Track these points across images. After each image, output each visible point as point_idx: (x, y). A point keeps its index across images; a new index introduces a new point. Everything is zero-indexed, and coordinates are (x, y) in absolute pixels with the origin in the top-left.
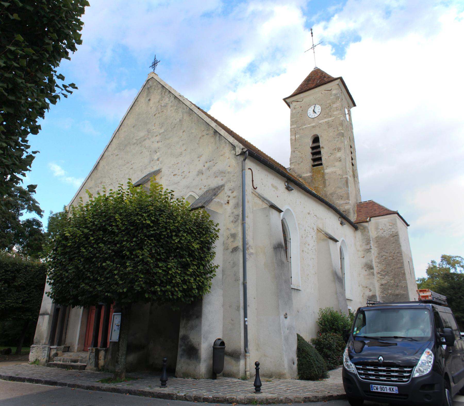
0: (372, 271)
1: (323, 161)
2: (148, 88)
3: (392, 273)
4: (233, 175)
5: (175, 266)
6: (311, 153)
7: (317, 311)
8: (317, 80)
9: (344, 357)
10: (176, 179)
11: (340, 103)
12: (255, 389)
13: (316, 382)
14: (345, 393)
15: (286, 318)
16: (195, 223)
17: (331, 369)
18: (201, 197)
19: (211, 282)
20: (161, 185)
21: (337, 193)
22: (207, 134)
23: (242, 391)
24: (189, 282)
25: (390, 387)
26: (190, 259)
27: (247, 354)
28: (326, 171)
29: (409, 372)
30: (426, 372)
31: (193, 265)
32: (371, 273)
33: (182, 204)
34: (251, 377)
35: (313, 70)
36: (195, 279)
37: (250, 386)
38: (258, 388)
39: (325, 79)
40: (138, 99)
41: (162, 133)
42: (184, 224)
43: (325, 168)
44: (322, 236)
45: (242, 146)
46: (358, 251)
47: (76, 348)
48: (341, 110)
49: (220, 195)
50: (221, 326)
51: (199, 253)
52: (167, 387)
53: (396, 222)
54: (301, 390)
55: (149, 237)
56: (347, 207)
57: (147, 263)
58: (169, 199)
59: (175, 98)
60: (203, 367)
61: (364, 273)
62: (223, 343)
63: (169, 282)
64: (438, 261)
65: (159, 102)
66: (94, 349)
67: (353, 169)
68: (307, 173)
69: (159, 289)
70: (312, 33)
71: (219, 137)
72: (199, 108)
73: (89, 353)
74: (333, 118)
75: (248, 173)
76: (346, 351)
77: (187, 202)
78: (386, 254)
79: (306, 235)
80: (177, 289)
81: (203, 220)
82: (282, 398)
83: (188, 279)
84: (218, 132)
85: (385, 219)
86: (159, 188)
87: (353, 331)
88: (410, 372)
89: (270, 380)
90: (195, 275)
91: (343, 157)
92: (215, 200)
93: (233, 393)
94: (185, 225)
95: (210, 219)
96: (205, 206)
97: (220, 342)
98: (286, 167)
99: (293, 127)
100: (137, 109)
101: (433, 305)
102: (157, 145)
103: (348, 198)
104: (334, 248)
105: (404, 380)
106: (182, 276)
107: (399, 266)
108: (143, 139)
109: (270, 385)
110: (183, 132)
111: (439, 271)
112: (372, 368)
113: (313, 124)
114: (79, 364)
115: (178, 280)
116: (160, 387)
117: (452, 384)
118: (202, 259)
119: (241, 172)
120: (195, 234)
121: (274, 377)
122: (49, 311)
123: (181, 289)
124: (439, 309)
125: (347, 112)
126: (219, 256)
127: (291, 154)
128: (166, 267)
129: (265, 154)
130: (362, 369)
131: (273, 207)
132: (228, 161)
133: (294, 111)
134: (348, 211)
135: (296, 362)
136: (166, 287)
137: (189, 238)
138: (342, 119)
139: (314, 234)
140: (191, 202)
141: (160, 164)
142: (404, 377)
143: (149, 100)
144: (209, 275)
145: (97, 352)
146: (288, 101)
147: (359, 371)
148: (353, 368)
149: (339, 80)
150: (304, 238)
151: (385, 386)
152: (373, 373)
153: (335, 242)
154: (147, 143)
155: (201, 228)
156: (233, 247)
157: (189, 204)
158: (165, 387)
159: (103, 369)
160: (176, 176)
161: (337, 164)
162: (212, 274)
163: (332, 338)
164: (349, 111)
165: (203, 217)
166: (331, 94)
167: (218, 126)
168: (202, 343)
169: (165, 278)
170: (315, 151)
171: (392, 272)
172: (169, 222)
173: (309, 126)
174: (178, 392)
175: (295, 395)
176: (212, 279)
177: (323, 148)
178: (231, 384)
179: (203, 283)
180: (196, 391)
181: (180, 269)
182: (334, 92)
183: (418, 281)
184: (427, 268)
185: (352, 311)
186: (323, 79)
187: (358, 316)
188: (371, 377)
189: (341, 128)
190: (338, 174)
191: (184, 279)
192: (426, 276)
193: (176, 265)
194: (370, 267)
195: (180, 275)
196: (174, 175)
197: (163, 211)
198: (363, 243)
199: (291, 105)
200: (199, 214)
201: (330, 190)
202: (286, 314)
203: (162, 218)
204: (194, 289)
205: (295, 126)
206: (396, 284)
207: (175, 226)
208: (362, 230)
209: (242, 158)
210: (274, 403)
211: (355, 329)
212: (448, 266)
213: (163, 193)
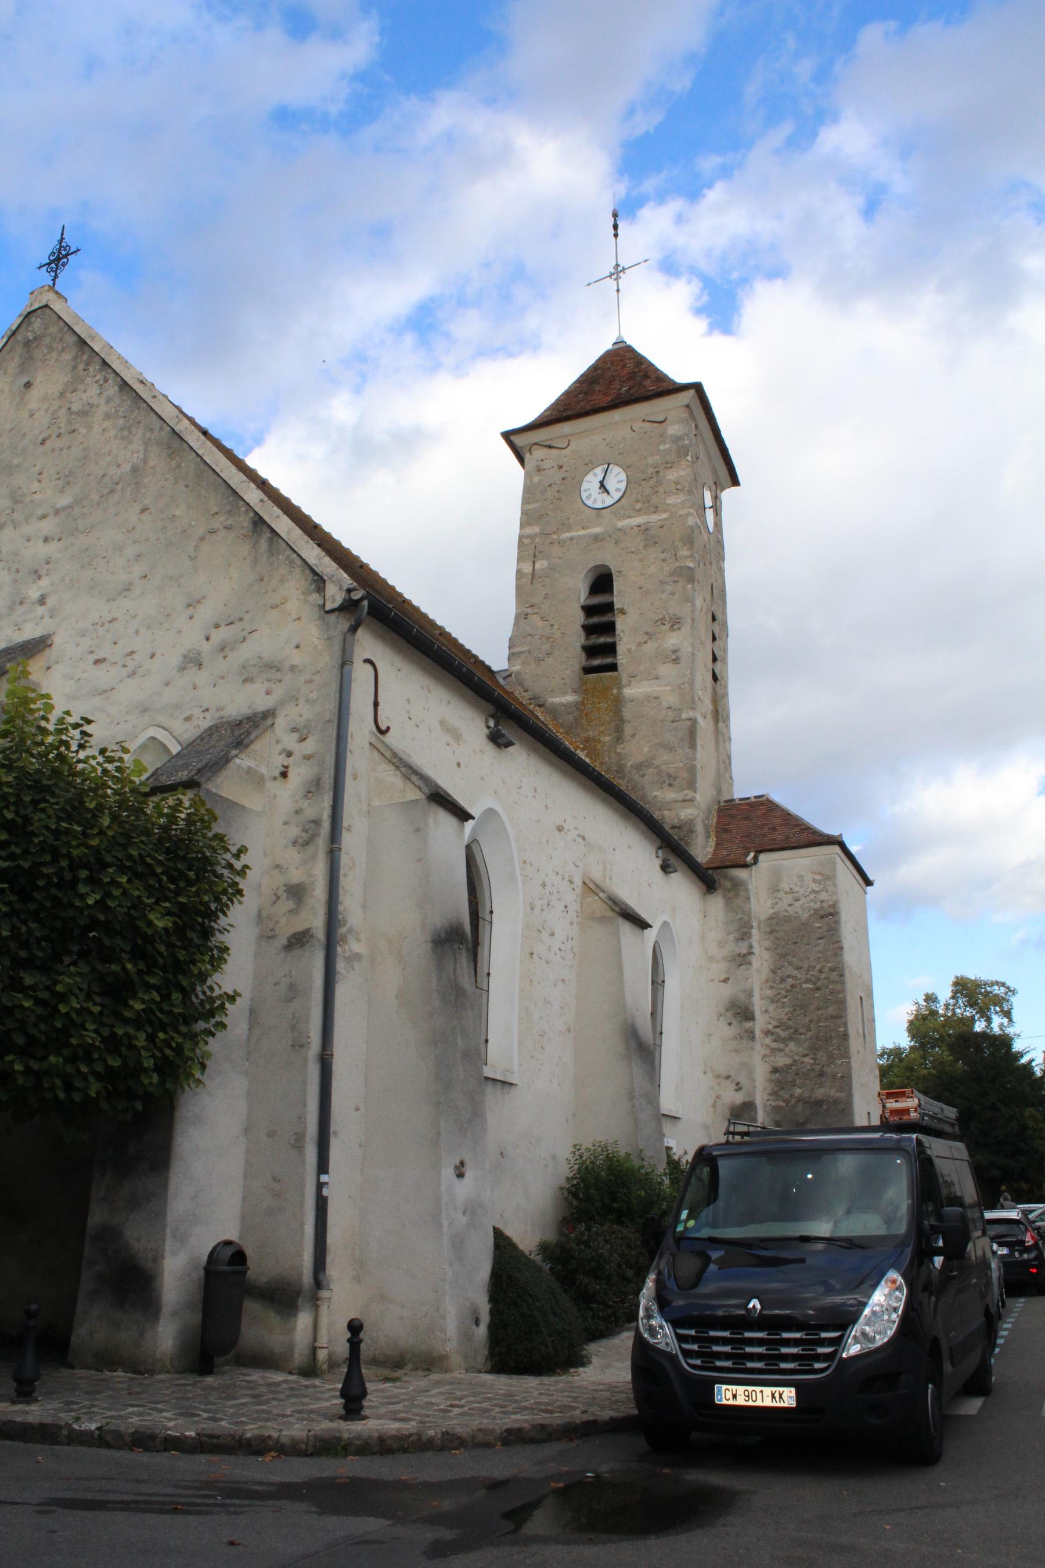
0: (748, 1025)
1: (622, 657)
2: (27, 344)
3: (810, 1034)
4: (307, 677)
5: (81, 989)
6: (584, 627)
7: (565, 1152)
8: (621, 382)
9: (643, 1302)
10: (103, 676)
11: (689, 470)
12: (345, 1407)
13: (547, 1380)
14: (636, 1412)
15: (460, 1175)
16: (160, 840)
17: (596, 1335)
18: (191, 748)
19: (207, 1048)
20: (48, 696)
21: (656, 763)
22: (228, 528)
23: (300, 1412)
24: (131, 1047)
25: (774, 1389)
26: (136, 965)
27: (324, 1294)
28: (628, 692)
29: (831, 1342)
30: (881, 1340)
31: (148, 987)
32: (746, 1032)
33: (118, 769)
34: (333, 1364)
35: (609, 346)
36: (151, 1038)
37: (327, 1395)
38: (353, 1402)
39: (647, 383)
41: (64, 508)
42: (121, 840)
43: (624, 682)
45: (347, 581)
46: (711, 959)
48: (690, 492)
49: (256, 746)
50: (237, 1200)
51: (170, 945)
52: (36, 1400)
53: (834, 870)
54: (496, 1405)
56: (686, 813)
58: (74, 748)
59: (121, 389)
60: (166, 1336)
61: (725, 1031)
62: (239, 1257)
64: (944, 994)
65: (62, 395)
67: (715, 692)
68: (564, 694)
69: (18, 1067)
71: (271, 541)
72: (205, 433)
74: (665, 516)
75: (361, 674)
76: (650, 1284)
77: (137, 762)
78: (795, 973)
79: (545, 902)
80: (84, 1069)
81: (190, 832)
82: (431, 1433)
83: (126, 1034)
84: (268, 524)
85: (802, 861)
86: (39, 704)
87: (677, 1221)
88: (837, 1342)
89: (396, 1374)
90: (151, 1023)
91: (686, 649)
92: (237, 761)
93: (268, 1420)
94: (125, 846)
95: (217, 828)
96: (202, 780)
97: (229, 1251)
98: (494, 668)
99: (528, 531)
101: (921, 1137)
102: (42, 550)
103: (692, 784)
104: (636, 948)
105: (818, 1366)
106: (104, 1025)
107: (831, 1010)
109: (396, 1391)
110: (143, 511)
111: (944, 1026)
112: (726, 1334)
113: (597, 530)
115: (90, 1036)
116: (14, 1402)
117: (947, 1367)
118: (179, 967)
119: (336, 672)
120: (160, 881)
121: (410, 1366)
123: (99, 1068)
124: (936, 1147)
125: (708, 502)
126: (243, 960)
127: (516, 624)
128: (47, 988)
129: (424, 616)
130: (694, 1340)
131: (440, 799)
132: (295, 630)
133: (536, 479)
134: (687, 827)
135: (485, 1318)
136: (45, 1058)
137: (136, 893)
138: (691, 521)
139: (571, 897)
140: (152, 763)
141: (47, 619)
142: (818, 1358)
143: (28, 385)
144: (201, 1025)
146: (513, 438)
147: (680, 1331)
148: (664, 1336)
149: (692, 392)
150: (537, 911)
151: (758, 1389)
152: (727, 1349)
153: (638, 930)
155: (183, 858)
156: (291, 932)
157: (146, 770)
158: (28, 1403)
160: (103, 666)
161: (666, 670)
162: (213, 1021)
163: (606, 1242)
164: (716, 498)
165: (190, 820)
166: (662, 436)
167: (269, 503)
168: (167, 1254)
169: (42, 1026)
170: (595, 620)
171: (809, 1030)
172: (68, 832)
173: (582, 532)
174: (77, 1419)
175: (476, 1422)
176: (210, 1039)
177: (622, 612)
178: (263, 1389)
179: (179, 1051)
180: (141, 1414)
181: (98, 999)
182: (673, 430)
183: (881, 1056)
184: (911, 1018)
185: (677, 1152)
186: (640, 384)
187: (698, 1171)
188: (719, 1363)
189: (685, 552)
190: (665, 705)
191: (113, 1035)
192: (905, 1041)
193: (85, 986)
195: (97, 1019)
196: (97, 662)
197: (48, 789)
198: (728, 934)
199: (527, 457)
200: (176, 808)
201: (635, 751)
202: (462, 1164)
203: (43, 816)
204: (146, 1070)
205: (537, 529)
206: (817, 1068)
207: (88, 847)
208: (729, 890)
209: (344, 624)
210: (405, 1450)
211: (684, 1215)
212: (969, 1012)
213: (51, 727)
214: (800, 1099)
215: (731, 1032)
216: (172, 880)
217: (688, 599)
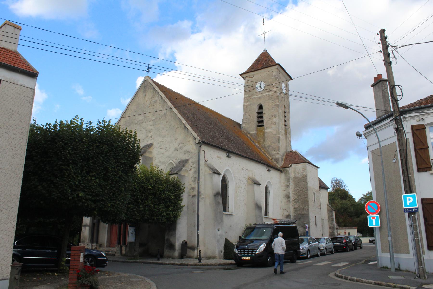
1: (265, 123)
2: (145, 87)
7: (244, 226)
10: (162, 151)
15: (219, 231)
28: (266, 131)
35: (263, 51)
40: (138, 93)
44: (250, 182)
47: (105, 245)
55: (150, 194)
56: (277, 156)
57: (150, 206)
60: (177, 254)
61: (285, 200)
62: (186, 243)
63: (160, 214)
65: (151, 98)
66: (119, 246)
70: (264, 22)
73: (116, 248)
75: (202, 153)
88: (256, 252)
100: (137, 100)
103: (279, 150)
107: (305, 196)
108: (141, 121)
114: (110, 253)
115: (164, 214)
118: (176, 203)
122: (89, 224)
127: (244, 116)
139: (245, 181)
143: (145, 95)
144: (179, 210)
145: (121, 247)
154: (144, 124)
159: (125, 255)
161: (273, 126)
166: (272, 75)
179: (176, 214)
182: (274, 74)
189: (277, 101)
194: (288, 197)
214: (299, 214)
215: (285, 201)
216: (174, 191)
217: (278, 111)
